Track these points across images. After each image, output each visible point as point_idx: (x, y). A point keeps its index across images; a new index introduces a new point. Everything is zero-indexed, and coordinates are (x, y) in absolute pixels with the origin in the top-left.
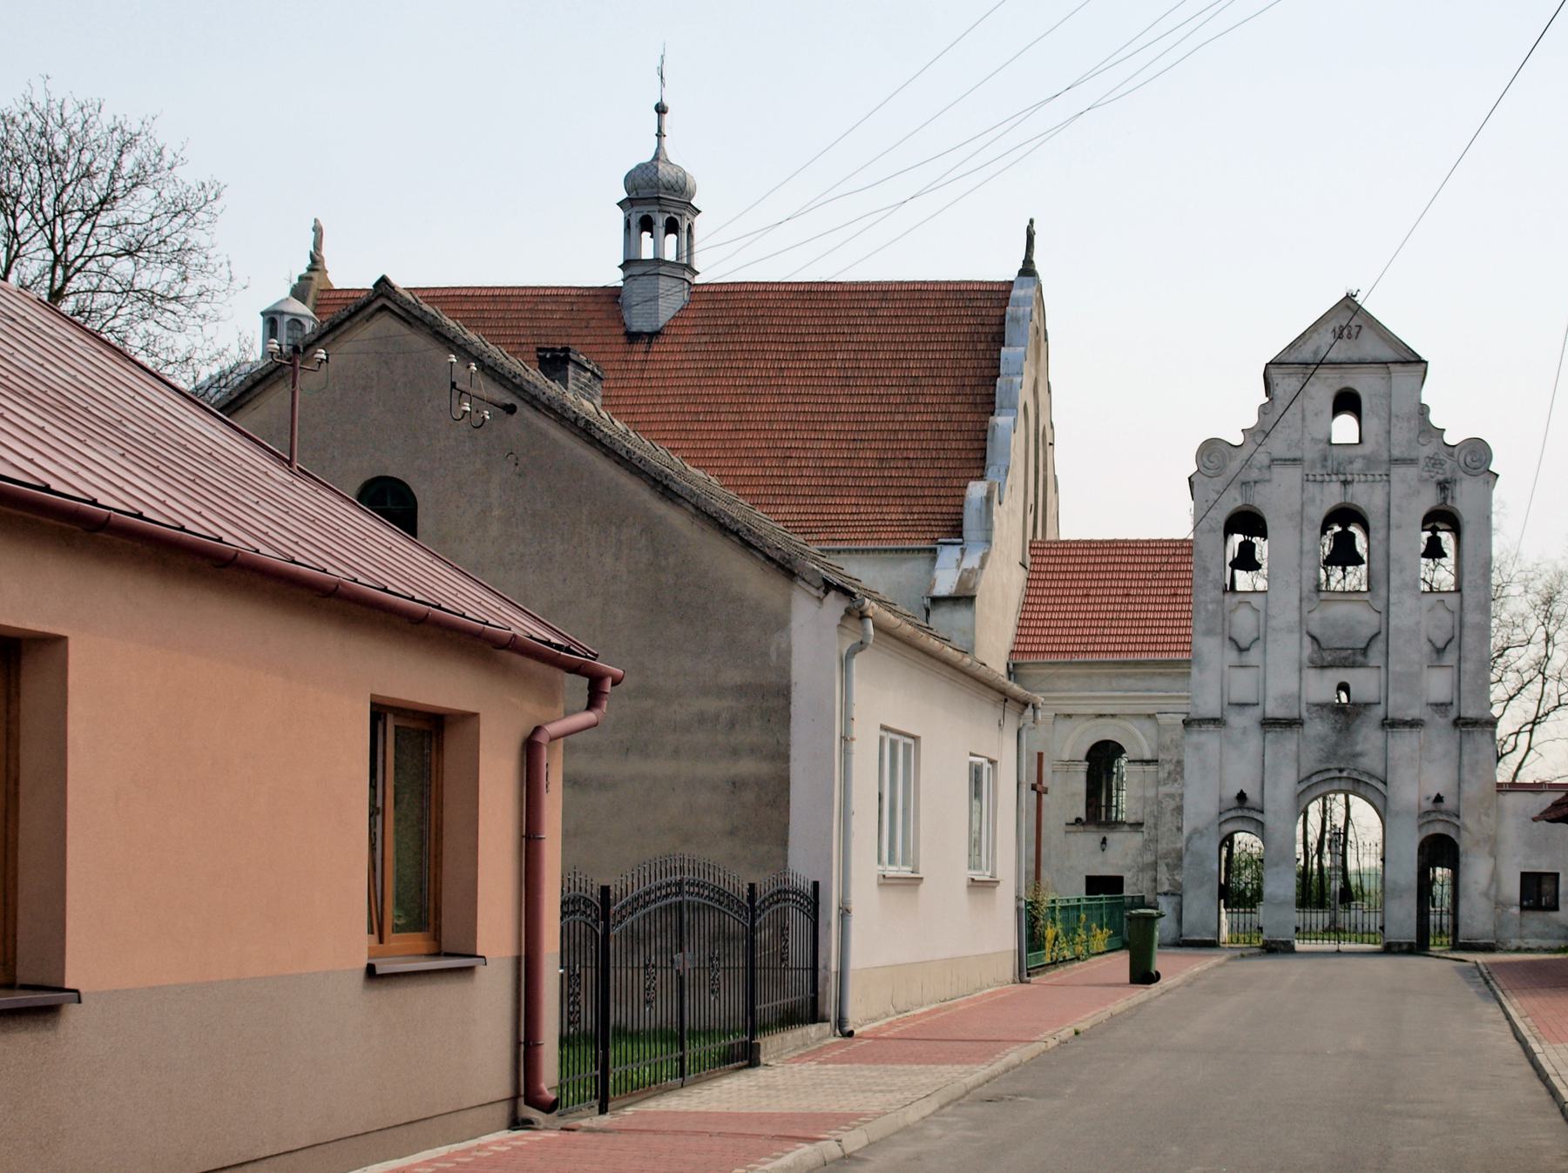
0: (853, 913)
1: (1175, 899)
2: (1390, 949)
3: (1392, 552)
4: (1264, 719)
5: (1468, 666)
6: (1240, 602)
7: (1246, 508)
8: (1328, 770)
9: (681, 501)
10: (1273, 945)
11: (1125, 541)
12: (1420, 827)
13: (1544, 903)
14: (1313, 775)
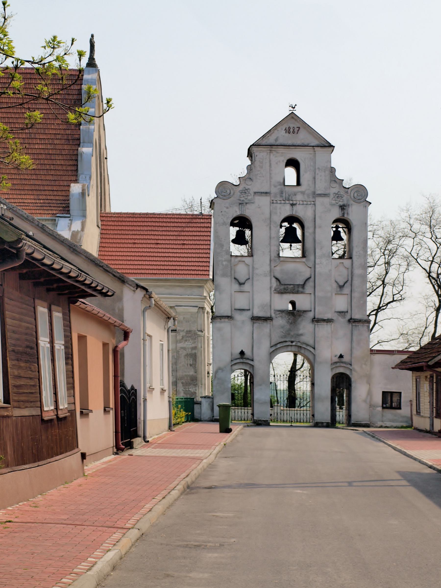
0: (147, 400)
1: (210, 400)
2: (317, 425)
3: (316, 239)
4: (253, 317)
5: (356, 295)
6: (239, 261)
7: (241, 215)
8: (286, 341)
9: (80, 255)
10: (260, 422)
11: (154, 214)
12: (332, 369)
13: (393, 406)
14: (278, 344)
